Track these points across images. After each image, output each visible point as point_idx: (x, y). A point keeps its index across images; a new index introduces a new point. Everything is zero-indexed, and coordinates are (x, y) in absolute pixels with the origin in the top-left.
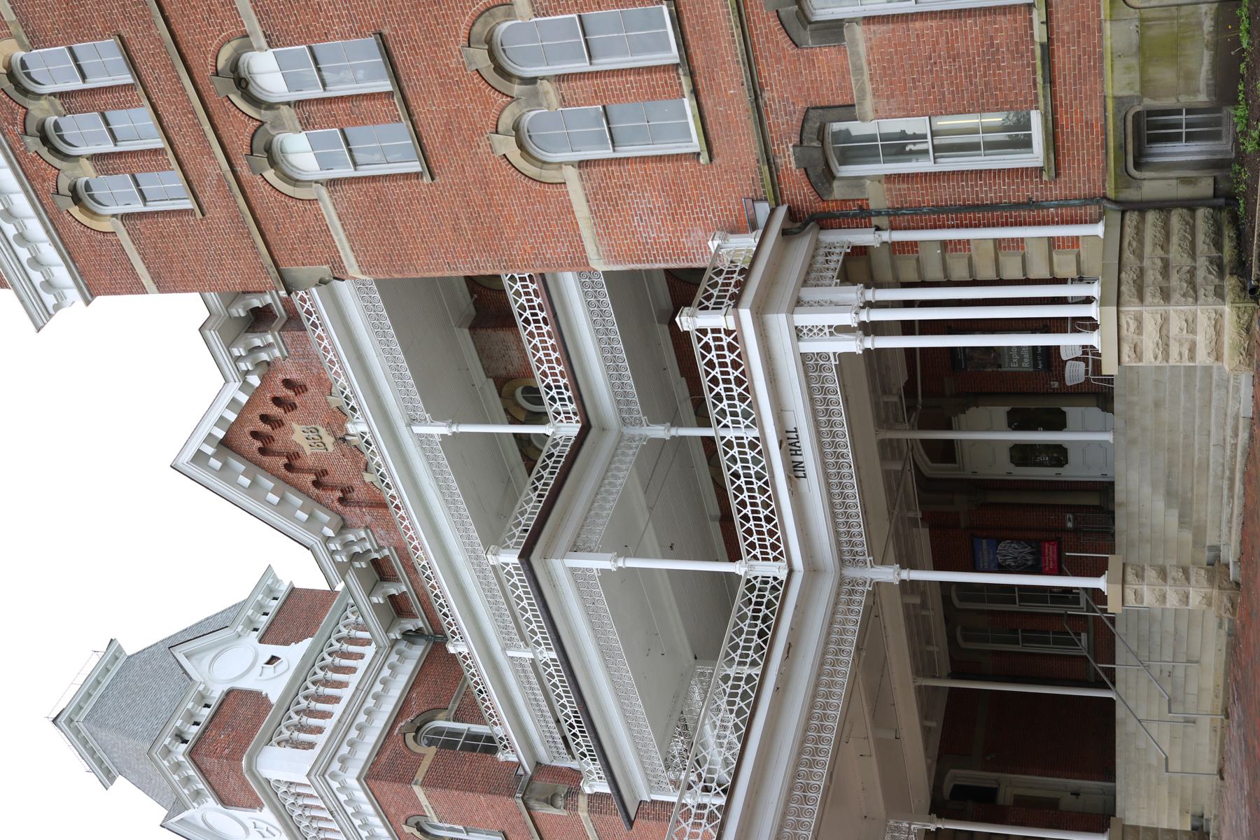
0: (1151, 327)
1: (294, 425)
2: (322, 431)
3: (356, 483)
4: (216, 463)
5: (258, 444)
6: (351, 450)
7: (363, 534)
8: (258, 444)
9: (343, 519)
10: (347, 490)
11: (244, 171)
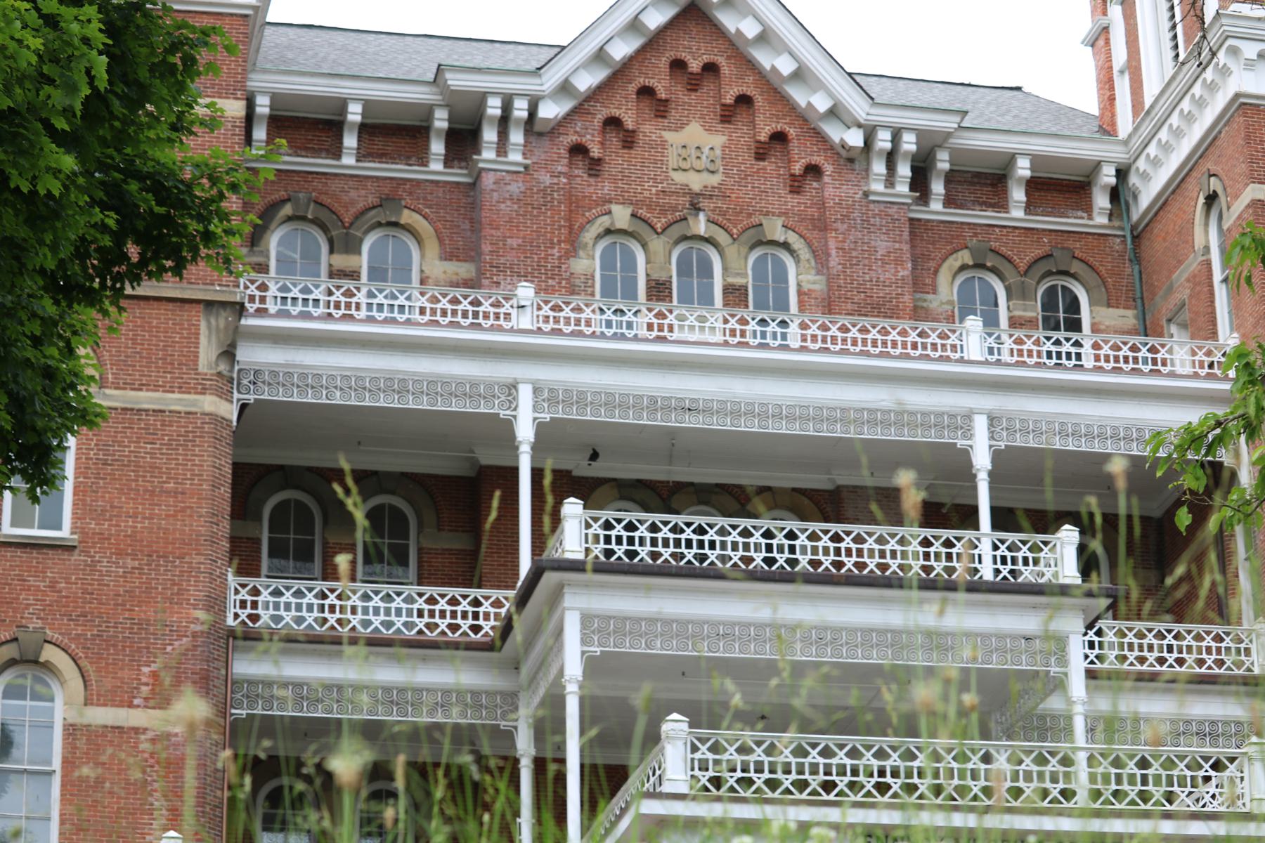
1: (718, 140)
2: (715, 180)
3: (606, 188)
5: (695, 66)
6: (674, 209)
7: (515, 156)
8: (695, 66)
9: (540, 134)
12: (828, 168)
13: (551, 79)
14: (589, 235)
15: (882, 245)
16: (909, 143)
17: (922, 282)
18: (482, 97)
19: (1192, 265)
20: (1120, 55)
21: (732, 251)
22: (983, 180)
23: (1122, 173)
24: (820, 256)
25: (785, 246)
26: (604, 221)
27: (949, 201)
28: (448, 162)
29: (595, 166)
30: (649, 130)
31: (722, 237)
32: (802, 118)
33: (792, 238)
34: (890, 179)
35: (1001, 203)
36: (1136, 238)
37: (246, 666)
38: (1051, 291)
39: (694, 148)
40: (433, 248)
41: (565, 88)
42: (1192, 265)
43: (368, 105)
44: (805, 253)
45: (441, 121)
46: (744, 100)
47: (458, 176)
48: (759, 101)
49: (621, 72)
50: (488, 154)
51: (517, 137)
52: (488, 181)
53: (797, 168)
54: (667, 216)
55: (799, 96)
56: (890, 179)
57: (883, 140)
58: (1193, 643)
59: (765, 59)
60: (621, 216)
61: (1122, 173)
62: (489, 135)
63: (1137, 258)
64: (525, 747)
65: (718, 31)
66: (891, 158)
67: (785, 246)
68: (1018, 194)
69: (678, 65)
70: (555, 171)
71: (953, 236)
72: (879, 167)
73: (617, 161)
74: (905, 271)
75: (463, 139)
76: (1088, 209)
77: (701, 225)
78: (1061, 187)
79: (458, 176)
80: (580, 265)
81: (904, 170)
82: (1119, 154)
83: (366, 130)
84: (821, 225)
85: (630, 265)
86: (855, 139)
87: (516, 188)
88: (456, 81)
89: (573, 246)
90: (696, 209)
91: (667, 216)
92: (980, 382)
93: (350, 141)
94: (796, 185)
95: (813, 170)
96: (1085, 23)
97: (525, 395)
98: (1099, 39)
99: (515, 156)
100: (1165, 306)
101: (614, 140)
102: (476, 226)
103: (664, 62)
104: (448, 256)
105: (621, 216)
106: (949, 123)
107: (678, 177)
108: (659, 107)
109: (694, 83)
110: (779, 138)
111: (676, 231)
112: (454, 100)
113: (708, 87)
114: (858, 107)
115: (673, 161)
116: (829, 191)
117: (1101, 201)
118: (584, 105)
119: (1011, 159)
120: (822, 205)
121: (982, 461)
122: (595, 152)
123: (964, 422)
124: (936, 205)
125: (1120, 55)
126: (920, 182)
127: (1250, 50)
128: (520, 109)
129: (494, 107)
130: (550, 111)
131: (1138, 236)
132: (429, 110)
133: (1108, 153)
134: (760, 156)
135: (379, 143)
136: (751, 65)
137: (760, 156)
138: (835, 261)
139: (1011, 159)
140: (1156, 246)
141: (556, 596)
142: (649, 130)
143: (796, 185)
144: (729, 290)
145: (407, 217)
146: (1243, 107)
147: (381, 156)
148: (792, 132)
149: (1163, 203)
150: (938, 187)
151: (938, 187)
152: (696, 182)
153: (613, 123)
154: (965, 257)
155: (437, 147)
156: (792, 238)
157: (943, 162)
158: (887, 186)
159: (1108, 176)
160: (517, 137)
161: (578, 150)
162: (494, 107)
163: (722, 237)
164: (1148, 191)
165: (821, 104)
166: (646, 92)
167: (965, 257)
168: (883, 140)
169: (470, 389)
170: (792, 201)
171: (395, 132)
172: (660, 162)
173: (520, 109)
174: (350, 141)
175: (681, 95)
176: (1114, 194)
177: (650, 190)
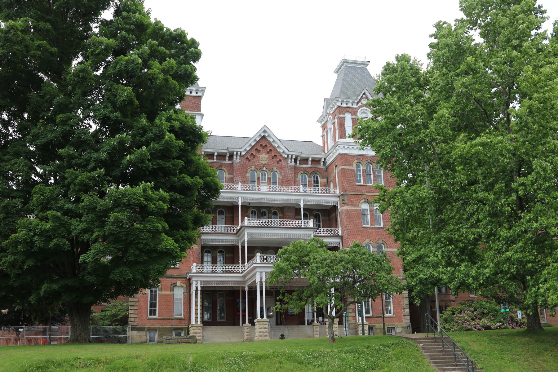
0: (199, 331)
1: (267, 156)
3: (251, 164)
4: (262, 135)
5: (264, 145)
7: (238, 160)
8: (264, 145)
10: (249, 161)
11: (364, 196)
14: (249, 171)
15: (290, 171)
16: (294, 157)
17: (295, 176)
18: (234, 152)
19: (333, 175)
20: (326, 140)
22: (305, 161)
23: (325, 159)
24: (281, 173)
27: (300, 164)
28: (229, 160)
29: (249, 161)
30: (257, 155)
31: (267, 170)
32: (279, 153)
34: (291, 162)
35: (307, 164)
36: (327, 168)
37: (203, 237)
38: (314, 177)
39: (264, 157)
40: (227, 173)
41: (245, 150)
42: (333, 175)
43: (217, 153)
45: (228, 155)
46: (271, 150)
47: (230, 162)
49: (253, 147)
50: (234, 160)
51: (238, 157)
52: (234, 163)
54: (260, 168)
55: (279, 150)
56: (291, 162)
57: (290, 156)
58: (333, 231)
59: (274, 144)
61: (325, 159)
62: (235, 157)
63: (327, 171)
64: (240, 247)
65: (267, 140)
66: (291, 159)
68: (310, 163)
69: (261, 145)
70: (244, 162)
71: (300, 169)
72: (290, 160)
73: (253, 160)
74: (293, 175)
75: (231, 156)
76: (320, 164)
77: (264, 169)
78: (316, 161)
79: (230, 162)
80: (247, 175)
81: (293, 160)
82: (325, 157)
83: (218, 156)
84: (281, 168)
85: (254, 175)
86: (286, 156)
87: (238, 164)
88: (230, 150)
89: (246, 172)
90: (264, 166)
91: (260, 168)
92: (303, 195)
93: (215, 158)
95: (280, 160)
96: (321, 134)
97: (240, 198)
98: (323, 136)
99: (238, 160)
100: (330, 179)
101: (252, 156)
102: (233, 170)
104: (229, 174)
105: (253, 168)
106: (300, 154)
108: (258, 151)
109: (263, 148)
112: (230, 152)
113: (266, 148)
114: (287, 152)
117: (322, 163)
118: (248, 152)
119: (309, 158)
121: (302, 206)
123: (300, 200)
124: (298, 165)
125: (326, 140)
126: (296, 160)
127: (342, 146)
128: (239, 154)
129: (235, 153)
131: (327, 168)
132: (226, 153)
133: (322, 156)
135: (219, 158)
136: (272, 145)
139: (309, 158)
140: (329, 170)
141: (244, 230)
142: (257, 155)
144: (268, 178)
145: (223, 168)
146: (340, 155)
147: (219, 159)
149: (330, 164)
150: (298, 162)
151: (298, 162)
152: (264, 162)
153: (252, 154)
154: (302, 172)
155: (227, 158)
157: (299, 159)
158: (291, 163)
159: (323, 160)
160: (238, 157)
161: (247, 158)
162: (235, 153)
164: (329, 162)
167: (302, 172)
168: (290, 156)
169: (233, 198)
170: (277, 165)
171: (221, 156)
173: (239, 154)
174: (215, 158)
175: (262, 150)
176: (324, 162)
177: (257, 164)
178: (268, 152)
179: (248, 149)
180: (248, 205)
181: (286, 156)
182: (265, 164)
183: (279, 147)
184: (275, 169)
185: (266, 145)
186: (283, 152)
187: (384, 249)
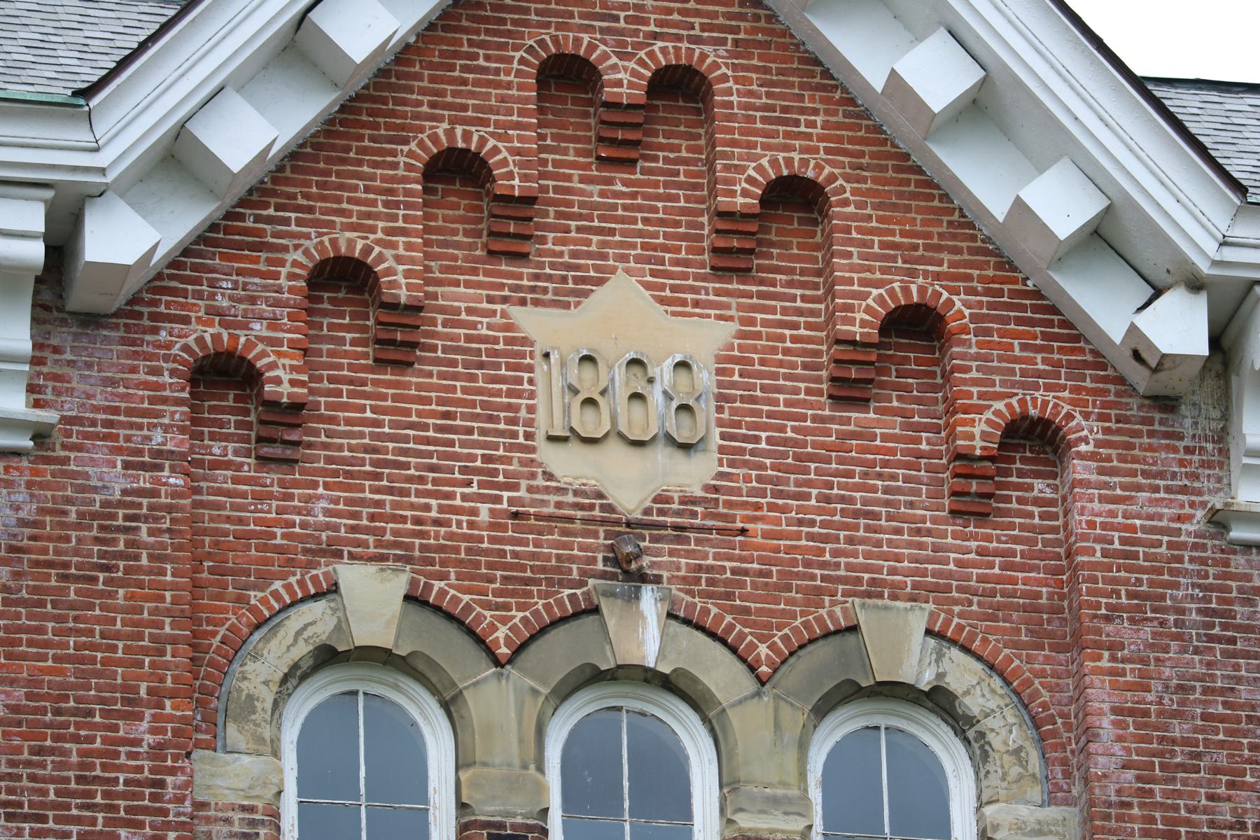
1: (706, 337)
3: (322, 506)
5: (624, 79)
8: (624, 79)
12: (1085, 431)
13: (127, 129)
21: (753, 721)
24: (1059, 737)
25: (939, 701)
26: (315, 620)
29: (281, 429)
30: (466, 301)
31: (719, 673)
32: (996, 257)
33: (962, 675)
41: (177, 158)
44: (1006, 729)
46: (794, 197)
48: (848, 202)
53: (978, 433)
55: (986, 180)
60: (371, 600)
67: (939, 701)
69: (567, 76)
73: (360, 412)
77: (644, 633)
84: (1062, 628)
86: (1179, 328)
89: (205, 708)
94: (975, 489)
95: (1034, 439)
101: (347, 341)
103: (516, 71)
105: (371, 600)
107: (568, 465)
110: (916, 325)
111: (561, 652)
113: (672, 149)
115: (550, 411)
116: (1089, 511)
118: (244, 218)
120: (1065, 563)
122: (283, 380)
130: (121, 239)
134: (849, 391)
136: (821, 74)
137: (849, 391)
138: (1109, 754)
142: (466, 301)
143: (975, 489)
148: (960, 306)
152: (629, 482)
153: (344, 277)
156: (962, 675)
163: (719, 673)
165: (1063, 207)
166: (456, 170)
170: (961, 546)
172: (505, 416)
178: (736, 251)
179: (247, 136)
180: (415, 304)
181: (1179, 328)
182: (669, 521)
183: (988, 107)
184: (903, 645)
185: (679, 87)
186: (1103, 238)
187: (141, 750)
